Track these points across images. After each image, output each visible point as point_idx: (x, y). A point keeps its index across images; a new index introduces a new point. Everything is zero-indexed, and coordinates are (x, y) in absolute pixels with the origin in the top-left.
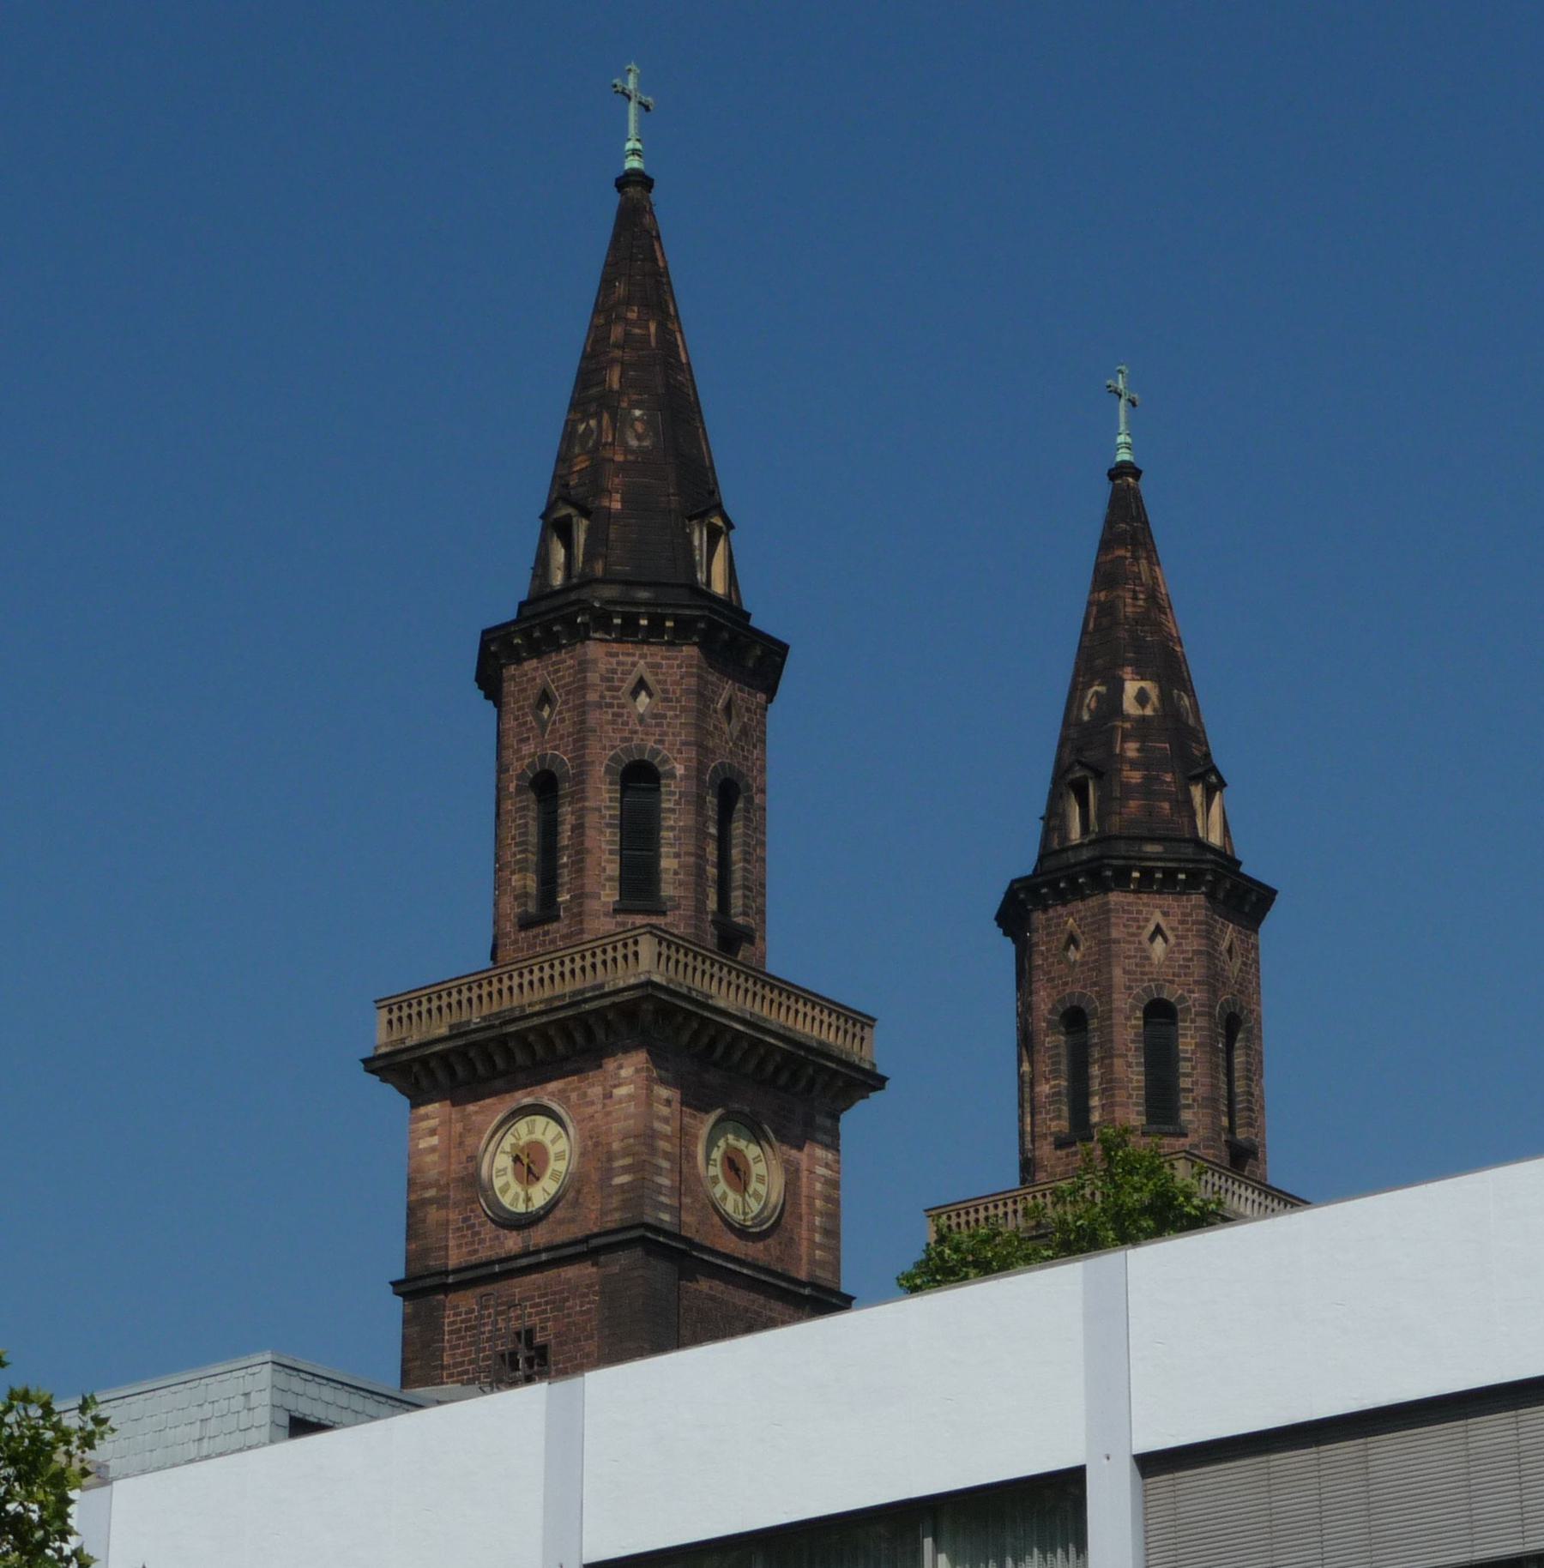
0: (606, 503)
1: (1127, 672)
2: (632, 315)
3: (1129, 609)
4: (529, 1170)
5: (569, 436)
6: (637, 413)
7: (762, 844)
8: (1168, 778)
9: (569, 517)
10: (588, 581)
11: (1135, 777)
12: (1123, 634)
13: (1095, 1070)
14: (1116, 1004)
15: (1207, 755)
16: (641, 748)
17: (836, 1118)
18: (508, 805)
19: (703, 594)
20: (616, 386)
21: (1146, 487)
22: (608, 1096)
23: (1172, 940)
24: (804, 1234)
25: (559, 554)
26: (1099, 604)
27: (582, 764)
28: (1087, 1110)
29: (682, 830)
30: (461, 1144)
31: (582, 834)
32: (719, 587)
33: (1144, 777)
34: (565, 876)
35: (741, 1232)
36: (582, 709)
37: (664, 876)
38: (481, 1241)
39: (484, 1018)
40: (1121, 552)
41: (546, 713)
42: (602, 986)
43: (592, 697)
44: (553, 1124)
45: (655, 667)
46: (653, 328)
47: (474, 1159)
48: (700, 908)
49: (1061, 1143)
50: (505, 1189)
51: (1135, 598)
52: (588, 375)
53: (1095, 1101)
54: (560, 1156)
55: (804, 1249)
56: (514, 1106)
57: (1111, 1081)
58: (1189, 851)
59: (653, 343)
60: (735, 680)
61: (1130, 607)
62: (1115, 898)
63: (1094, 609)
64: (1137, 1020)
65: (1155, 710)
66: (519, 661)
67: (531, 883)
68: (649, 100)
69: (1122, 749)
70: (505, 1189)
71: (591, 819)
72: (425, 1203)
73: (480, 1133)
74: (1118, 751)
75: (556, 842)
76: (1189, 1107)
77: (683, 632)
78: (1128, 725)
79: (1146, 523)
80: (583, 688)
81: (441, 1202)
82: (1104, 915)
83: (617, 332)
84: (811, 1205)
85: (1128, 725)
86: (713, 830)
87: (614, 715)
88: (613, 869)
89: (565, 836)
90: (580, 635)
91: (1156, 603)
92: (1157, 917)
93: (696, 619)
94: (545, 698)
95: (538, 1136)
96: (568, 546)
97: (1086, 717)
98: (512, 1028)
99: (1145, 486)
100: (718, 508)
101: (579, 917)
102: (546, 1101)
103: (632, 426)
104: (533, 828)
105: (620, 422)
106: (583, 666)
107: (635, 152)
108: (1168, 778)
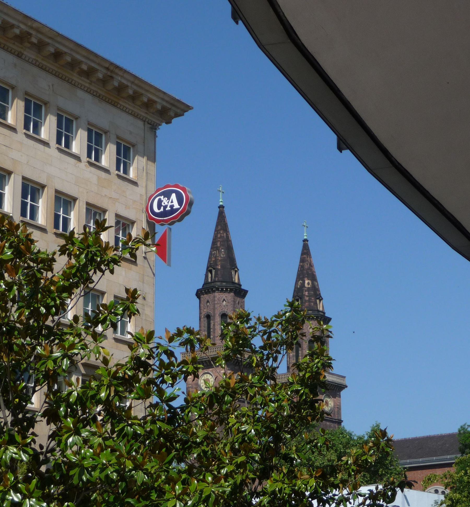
0: (218, 267)
1: (306, 279)
2: (222, 232)
5: (211, 254)
6: (223, 250)
8: (313, 299)
9: (212, 270)
10: (215, 281)
11: (307, 298)
12: (305, 272)
13: (300, 352)
15: (320, 294)
16: (224, 311)
18: (202, 320)
19: (234, 283)
20: (219, 246)
21: (309, 243)
25: (210, 275)
26: (301, 265)
27: (214, 313)
32: (237, 281)
34: (212, 333)
36: (214, 304)
40: (305, 256)
41: (208, 304)
43: (216, 302)
45: (226, 297)
46: (225, 234)
50: (203, 386)
51: (307, 265)
52: (214, 243)
56: (204, 372)
58: (316, 313)
60: (240, 297)
61: (306, 266)
66: (203, 295)
67: (206, 333)
68: (223, 191)
70: (203, 386)
71: (216, 324)
72: (189, 387)
77: (231, 290)
79: (309, 250)
81: (192, 388)
83: (219, 236)
85: (306, 289)
89: (212, 327)
90: (214, 292)
91: (311, 265)
93: (233, 289)
94: (208, 302)
95: (208, 377)
96: (211, 274)
97: (299, 287)
98: (204, 360)
99: (309, 243)
100: (236, 267)
104: (206, 324)
105: (220, 252)
106: (214, 297)
107: (221, 201)
108: (313, 299)
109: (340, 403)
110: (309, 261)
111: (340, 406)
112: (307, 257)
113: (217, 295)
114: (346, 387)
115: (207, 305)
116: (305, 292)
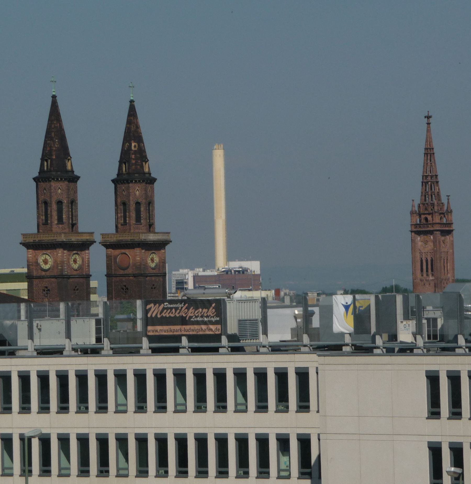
1: (132, 142)
3: (133, 129)
4: (46, 263)
6: (57, 140)
7: (77, 209)
10: (51, 171)
11: (134, 162)
13: (127, 214)
14: (131, 203)
16: (60, 199)
20: (53, 136)
21: (136, 104)
22: (57, 255)
23: (140, 191)
25: (46, 163)
27: (51, 201)
28: (126, 220)
29: (66, 211)
30: (35, 257)
31: (52, 213)
33: (135, 162)
34: (49, 219)
35: (76, 270)
36: (51, 193)
37: (64, 218)
39: (39, 240)
42: (56, 240)
43: (52, 191)
44: (49, 257)
46: (58, 124)
47: (37, 259)
48: (69, 223)
49: (122, 225)
50: (42, 265)
51: (134, 127)
53: (127, 219)
54: (50, 262)
55: (84, 269)
57: (130, 216)
59: (59, 128)
61: (133, 129)
62: (131, 185)
63: (127, 128)
64: (134, 206)
65: (137, 149)
69: (132, 157)
70: (42, 265)
71: (53, 210)
74: (131, 157)
75: (47, 213)
76: (142, 220)
78: (133, 152)
80: (51, 190)
81: (32, 265)
82: (128, 189)
84: (85, 263)
85: (133, 152)
86: (70, 210)
87: (56, 194)
88: (56, 218)
91: (138, 127)
92: (137, 188)
98: (43, 243)
101: (51, 225)
102: (48, 253)
103: (56, 143)
106: (50, 186)
109: (165, 257)
110: (136, 123)
111: (165, 260)
112: (134, 119)
113: (53, 184)
114: (171, 242)
115: (44, 192)
116: (132, 155)
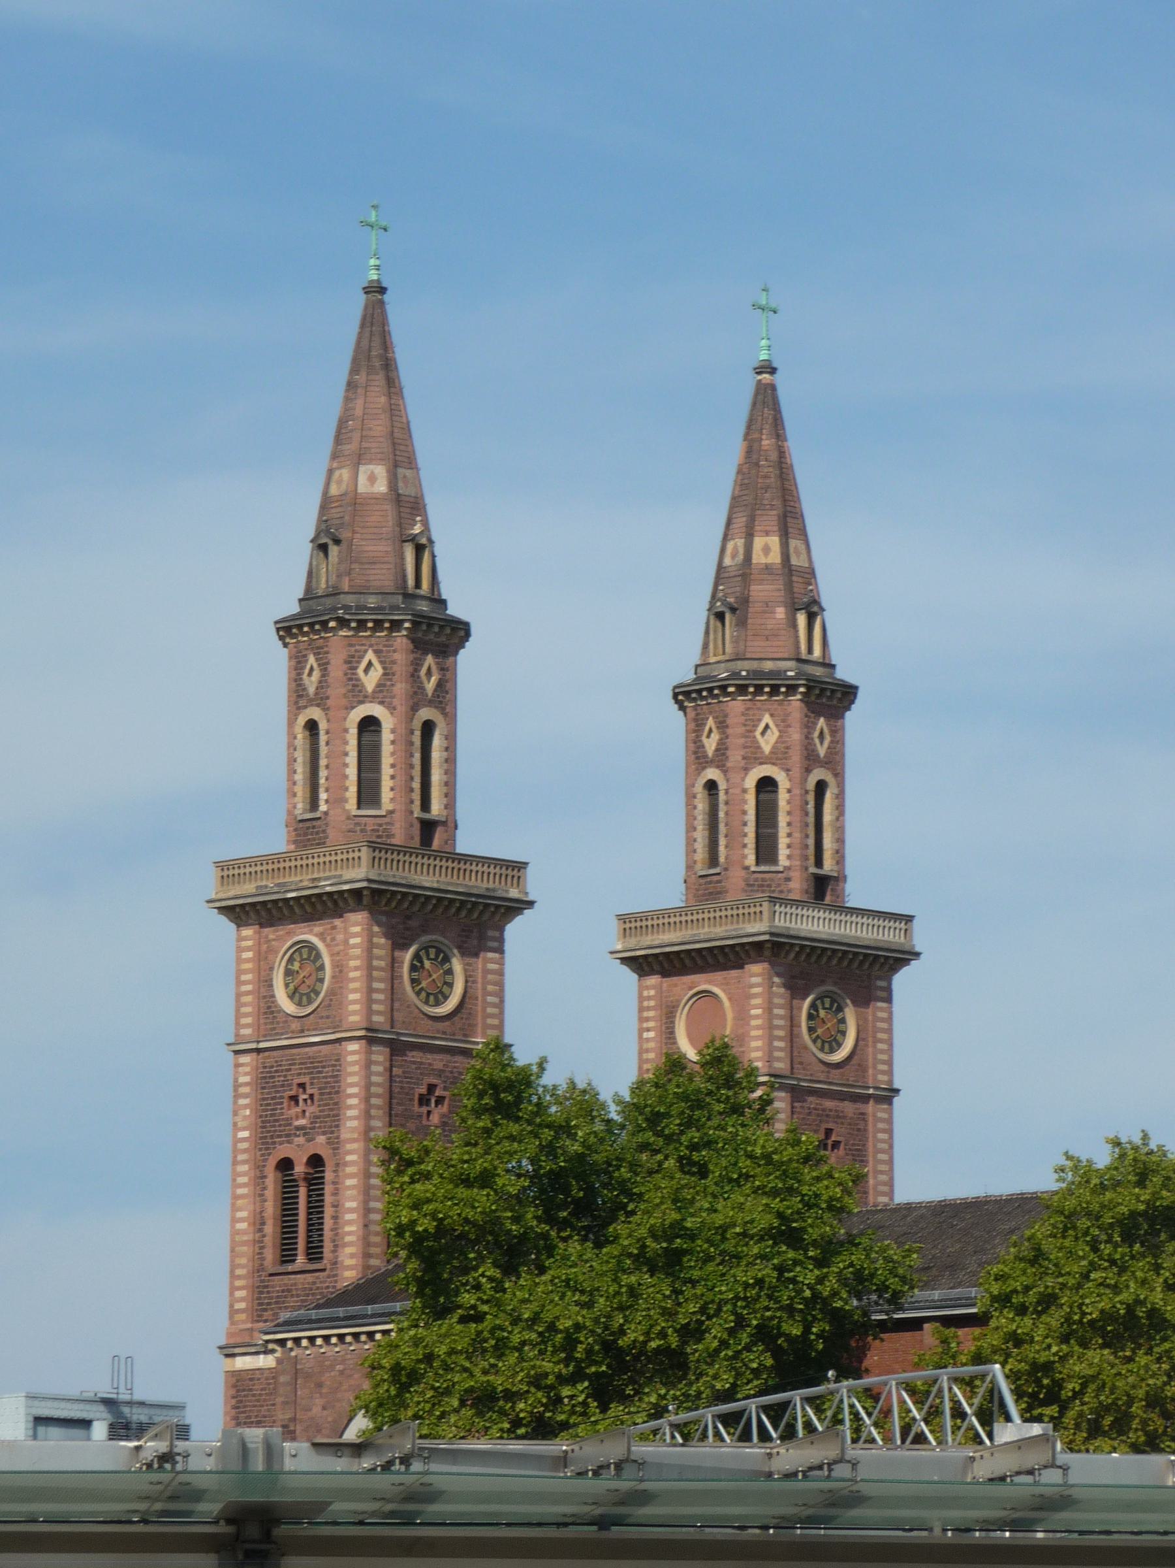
17: (501, 930)
24: (479, 1008)
38: (278, 1023)
73: (277, 952)
